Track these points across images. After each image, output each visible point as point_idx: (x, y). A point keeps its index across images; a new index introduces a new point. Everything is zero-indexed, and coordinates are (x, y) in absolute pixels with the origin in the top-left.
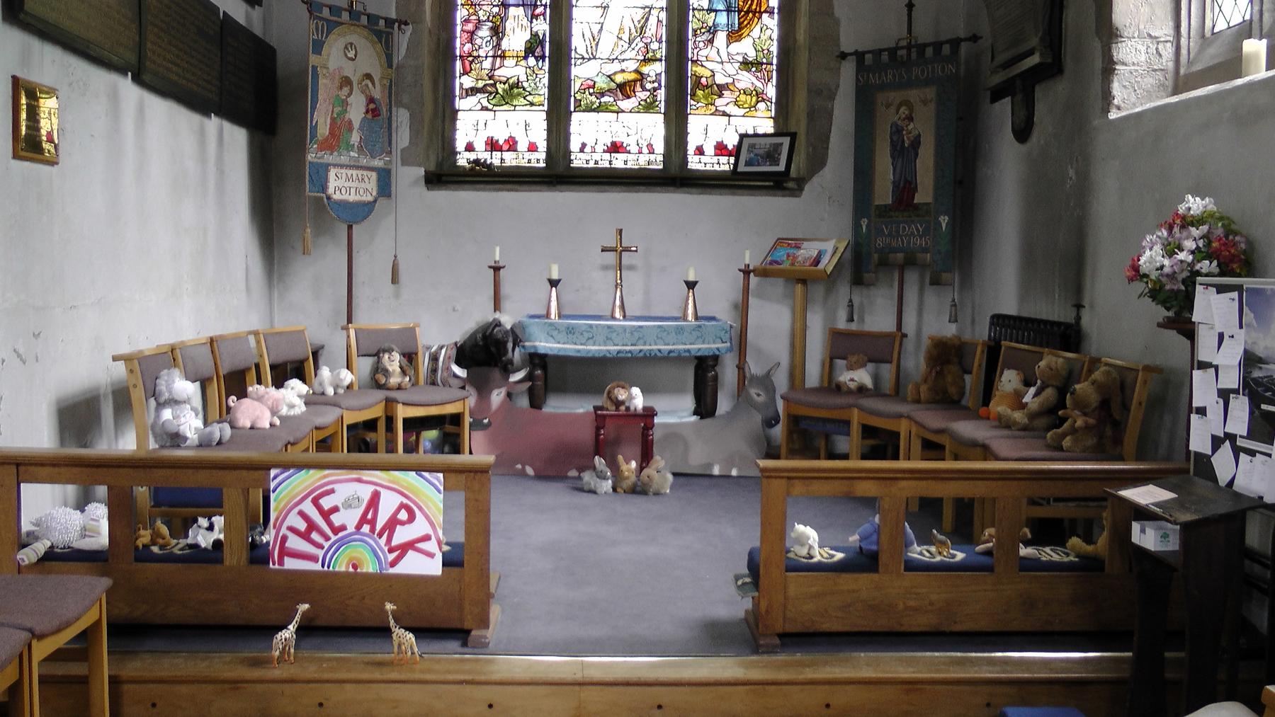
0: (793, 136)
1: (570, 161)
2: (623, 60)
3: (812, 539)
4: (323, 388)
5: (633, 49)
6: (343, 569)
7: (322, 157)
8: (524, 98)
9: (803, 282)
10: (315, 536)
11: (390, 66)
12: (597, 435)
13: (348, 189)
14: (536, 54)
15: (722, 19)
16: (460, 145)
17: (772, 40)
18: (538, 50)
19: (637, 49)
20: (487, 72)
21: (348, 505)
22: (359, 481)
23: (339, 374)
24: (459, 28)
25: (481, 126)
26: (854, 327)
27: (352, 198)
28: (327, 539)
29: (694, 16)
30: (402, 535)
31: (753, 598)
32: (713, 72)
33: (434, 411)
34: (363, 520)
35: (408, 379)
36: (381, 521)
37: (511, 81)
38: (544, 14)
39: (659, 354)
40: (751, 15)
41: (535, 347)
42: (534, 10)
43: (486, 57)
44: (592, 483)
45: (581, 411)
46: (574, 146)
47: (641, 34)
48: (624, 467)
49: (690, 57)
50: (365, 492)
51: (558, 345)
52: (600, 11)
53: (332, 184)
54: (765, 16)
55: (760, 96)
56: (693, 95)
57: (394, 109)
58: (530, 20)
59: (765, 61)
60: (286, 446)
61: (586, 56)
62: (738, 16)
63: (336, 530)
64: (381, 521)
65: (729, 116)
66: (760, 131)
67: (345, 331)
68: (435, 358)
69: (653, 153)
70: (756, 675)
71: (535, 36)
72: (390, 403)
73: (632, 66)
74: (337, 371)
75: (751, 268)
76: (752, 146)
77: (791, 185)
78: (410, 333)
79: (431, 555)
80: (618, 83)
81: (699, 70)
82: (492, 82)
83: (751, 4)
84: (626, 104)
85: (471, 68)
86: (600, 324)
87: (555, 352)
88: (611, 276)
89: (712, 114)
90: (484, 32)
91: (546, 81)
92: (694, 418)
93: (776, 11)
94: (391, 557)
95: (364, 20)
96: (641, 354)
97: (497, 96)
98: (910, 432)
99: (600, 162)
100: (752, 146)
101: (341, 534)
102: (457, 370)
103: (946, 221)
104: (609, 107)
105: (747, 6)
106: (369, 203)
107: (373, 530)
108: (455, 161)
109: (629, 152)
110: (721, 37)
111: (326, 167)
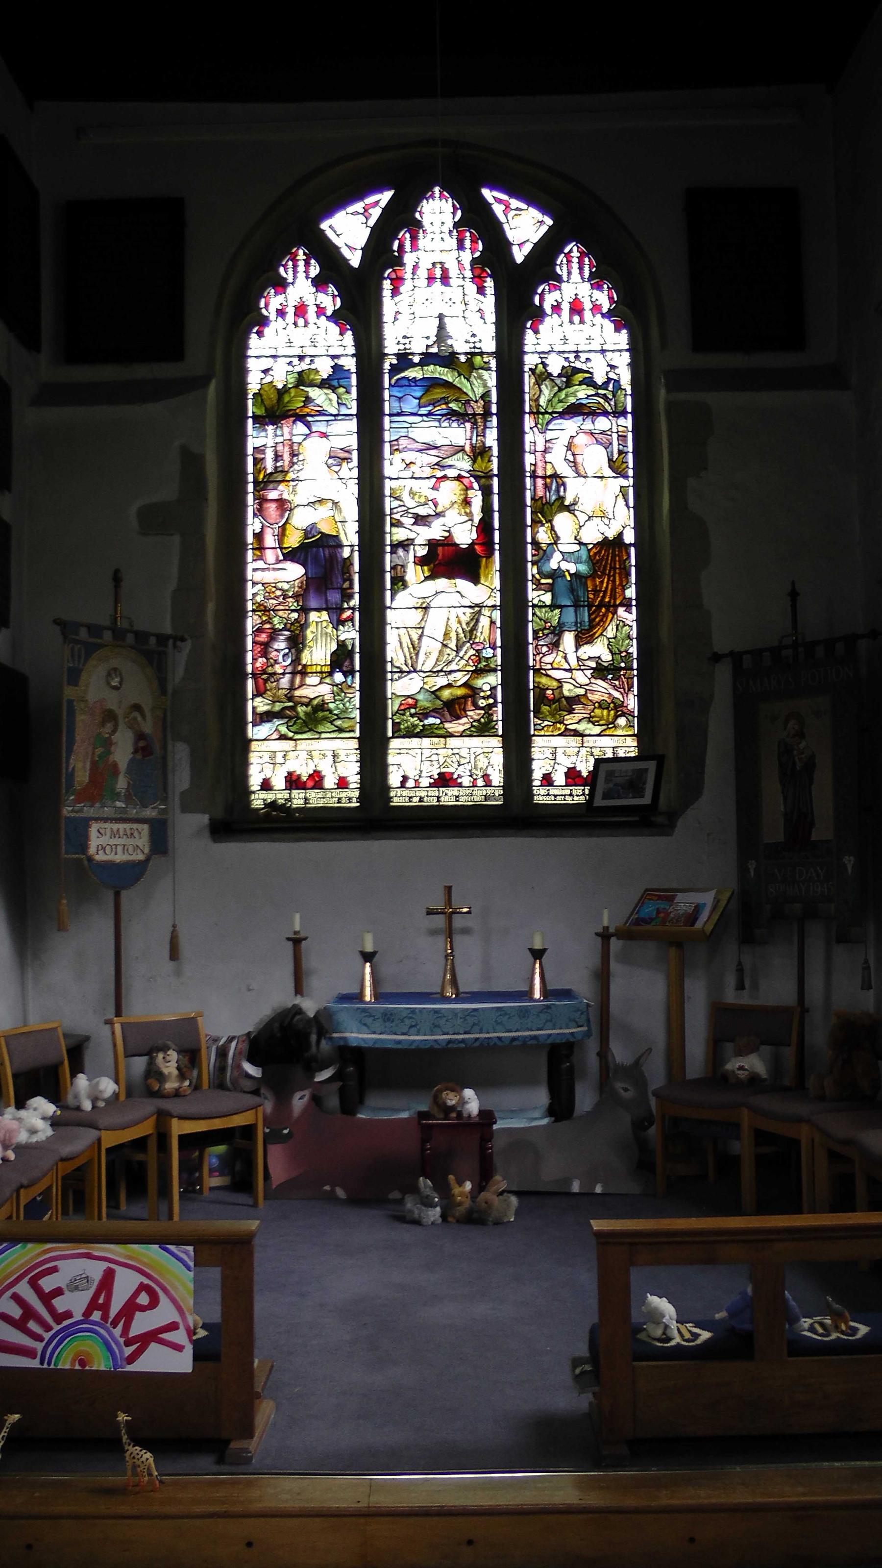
0: (661, 760)
1: (390, 799)
2: (451, 672)
3: (667, 1317)
4: (79, 1101)
5: (462, 658)
6: (68, 1366)
7: (81, 811)
8: (331, 723)
9: (679, 945)
10: (32, 1325)
11: (164, 692)
12: (423, 1150)
13: (113, 847)
14: (345, 669)
15: (570, 616)
16: (255, 782)
17: (632, 640)
18: (346, 664)
19: (466, 658)
20: (285, 692)
21: (74, 1286)
22: (89, 1256)
23: (97, 1084)
24: (249, 640)
25: (279, 759)
26: (745, 999)
27: (119, 857)
28: (48, 1328)
29: (534, 614)
30: (142, 1324)
31: (594, 1393)
32: (561, 683)
33: (217, 1124)
34: (93, 1306)
35: (187, 1083)
36: (116, 1306)
37: (315, 702)
38: (351, 619)
39: (499, 1043)
40: (603, 610)
41: (345, 1039)
42: (341, 615)
43: (283, 674)
44: (416, 1212)
45: (405, 1115)
46: (394, 780)
47: (470, 639)
48: (456, 1190)
49: (531, 664)
50: (96, 1270)
51: (374, 1036)
52: (419, 614)
53: (95, 841)
54: (621, 611)
55: (619, 709)
56: (537, 712)
57: (170, 742)
58: (335, 626)
59: (623, 665)
60: (18, 1192)
61: (405, 668)
62: (589, 611)
63: (59, 1317)
64: (116, 1306)
65: (582, 735)
66: (621, 754)
67: (108, 1026)
68: (222, 1053)
69: (491, 786)
70: (594, 1500)
71: (342, 645)
72: (163, 1118)
73: (461, 678)
74: (98, 1079)
75: (612, 930)
76: (610, 774)
77: (660, 819)
78: (190, 1024)
79: (179, 1348)
80: (445, 700)
81: (544, 680)
82: (291, 704)
83: (604, 597)
84: (454, 727)
85: (265, 687)
86: (425, 1008)
87: (370, 1044)
88: (441, 940)
89: (559, 735)
90: (281, 644)
91: (357, 702)
92: (545, 1121)
93: (634, 603)
94: (128, 1351)
95: (130, 638)
96: (477, 1044)
97: (298, 721)
98: (813, 1141)
99: (426, 799)
100: (610, 774)
101: (65, 1323)
102: (250, 1069)
103: (852, 862)
104: (436, 731)
105: (599, 599)
106: (140, 862)
107: (105, 1317)
108: (249, 802)
109: (460, 785)
110: (568, 639)
111: (86, 823)
